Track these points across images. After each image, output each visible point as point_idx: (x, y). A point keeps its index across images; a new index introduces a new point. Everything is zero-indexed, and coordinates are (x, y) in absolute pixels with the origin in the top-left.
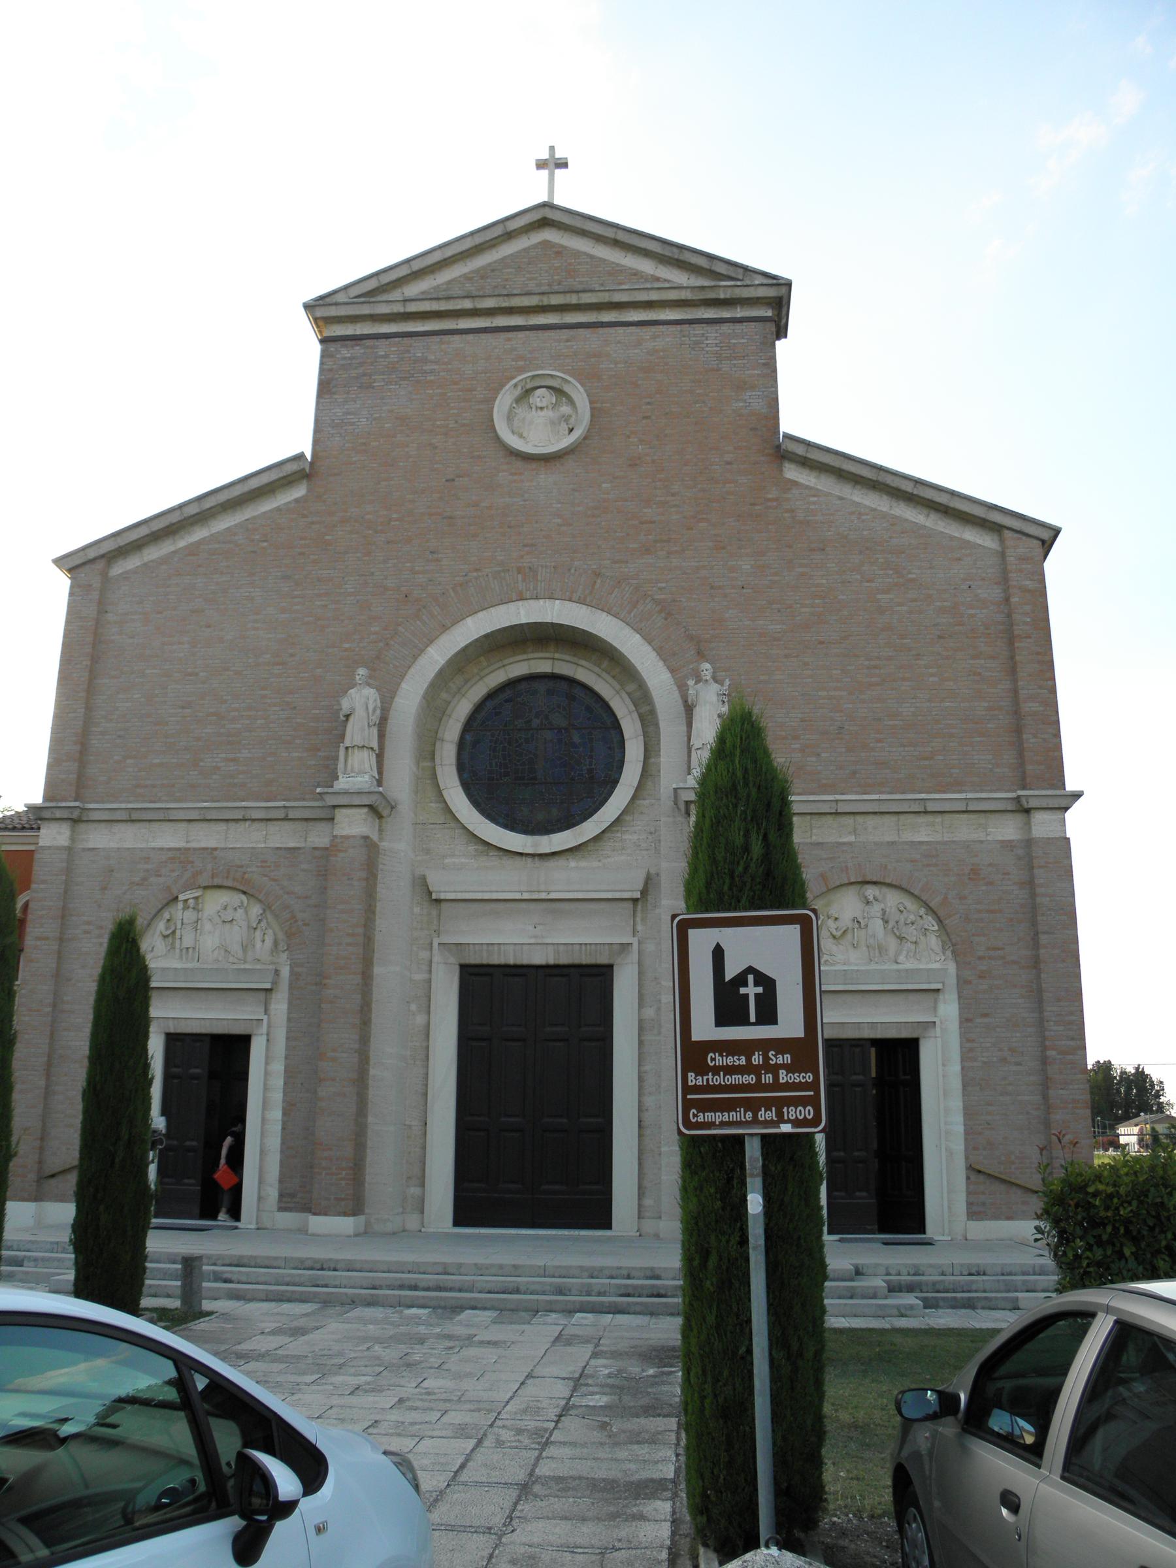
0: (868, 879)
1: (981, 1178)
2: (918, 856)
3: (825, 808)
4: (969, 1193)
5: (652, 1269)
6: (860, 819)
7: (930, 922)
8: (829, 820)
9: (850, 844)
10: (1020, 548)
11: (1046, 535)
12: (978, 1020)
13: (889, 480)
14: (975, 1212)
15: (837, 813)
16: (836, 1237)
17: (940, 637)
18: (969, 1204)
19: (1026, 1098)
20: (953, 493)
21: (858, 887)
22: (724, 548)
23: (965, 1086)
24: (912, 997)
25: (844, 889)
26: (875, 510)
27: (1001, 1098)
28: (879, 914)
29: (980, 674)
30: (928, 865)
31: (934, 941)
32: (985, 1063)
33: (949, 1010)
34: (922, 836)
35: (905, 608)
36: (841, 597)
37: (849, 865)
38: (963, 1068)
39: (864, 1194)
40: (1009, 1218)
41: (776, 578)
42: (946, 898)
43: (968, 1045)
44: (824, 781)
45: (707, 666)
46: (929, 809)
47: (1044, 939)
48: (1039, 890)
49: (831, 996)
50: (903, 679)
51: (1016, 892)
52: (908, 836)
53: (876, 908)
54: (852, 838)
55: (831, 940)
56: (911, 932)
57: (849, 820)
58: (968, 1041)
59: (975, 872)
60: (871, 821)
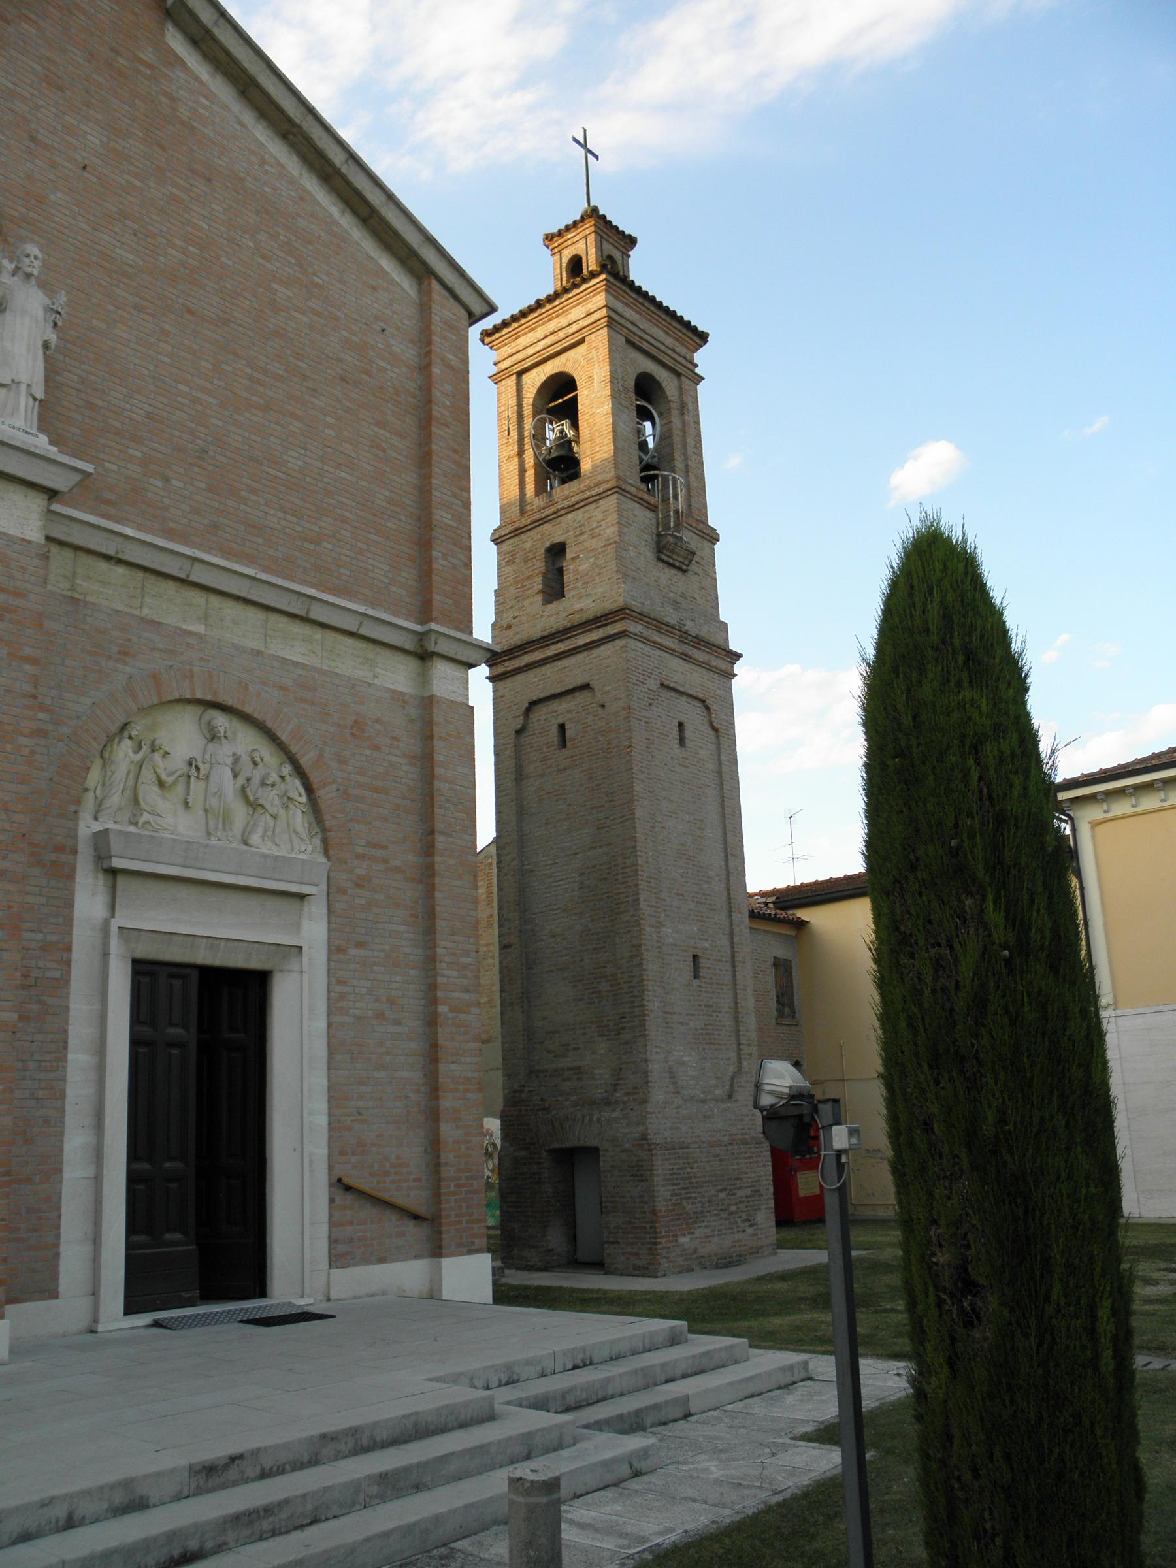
0: (222, 698)
1: (349, 1197)
2: (290, 683)
3: (172, 567)
4: (332, 1224)
5: (127, 1484)
6: (215, 601)
7: (295, 787)
8: (170, 588)
9: (200, 637)
10: (444, 310)
11: (477, 308)
12: (352, 952)
13: (316, 133)
14: (341, 1255)
15: (184, 582)
16: (146, 1318)
17: (343, 379)
18: (333, 1241)
19: (406, 1074)
20: (390, 197)
21: (198, 710)
22: (61, 89)
23: (331, 1053)
24: (272, 903)
25: (179, 707)
26: (282, 166)
27: (376, 1074)
28: (229, 761)
29: (384, 450)
30: (302, 700)
31: (299, 819)
32: (358, 1018)
33: (313, 931)
34: (297, 653)
35: (305, 319)
36: (224, 259)
37: (196, 669)
38: (329, 1025)
39: (178, 1236)
40: (381, 1260)
41: (138, 184)
42: (321, 756)
43: (339, 988)
44: (171, 524)
45: (648, 425)
46: (312, 616)
47: (440, 839)
48: (438, 771)
49: (135, 884)
50: (293, 416)
51: (405, 768)
52: (276, 648)
53: (224, 752)
54: (201, 629)
55: (156, 788)
56: (270, 798)
57: (198, 598)
58: (340, 982)
59: (358, 724)
60: (231, 610)
